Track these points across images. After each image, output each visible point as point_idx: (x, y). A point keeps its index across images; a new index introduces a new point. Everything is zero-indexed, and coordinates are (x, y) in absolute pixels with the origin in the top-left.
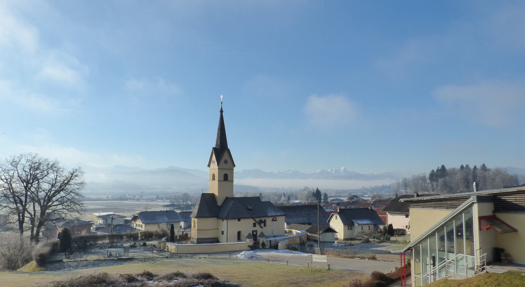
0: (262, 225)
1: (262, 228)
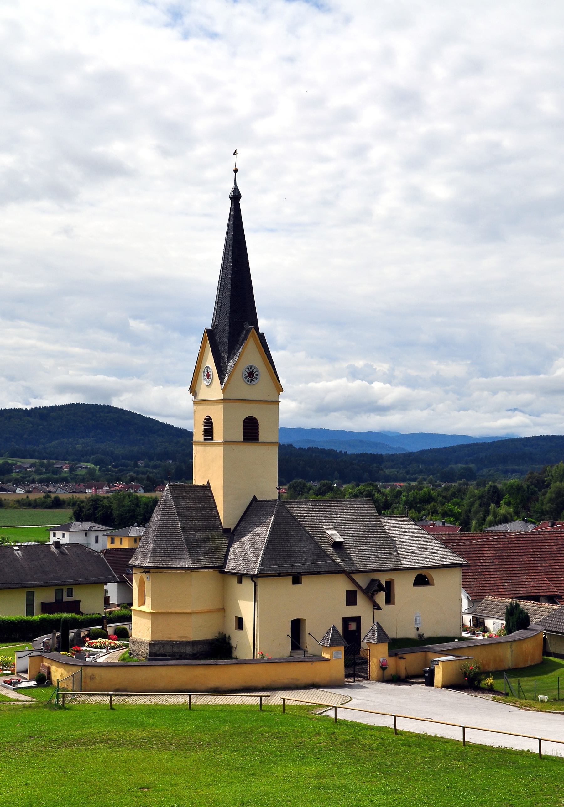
0: (381, 598)
1: (380, 609)
